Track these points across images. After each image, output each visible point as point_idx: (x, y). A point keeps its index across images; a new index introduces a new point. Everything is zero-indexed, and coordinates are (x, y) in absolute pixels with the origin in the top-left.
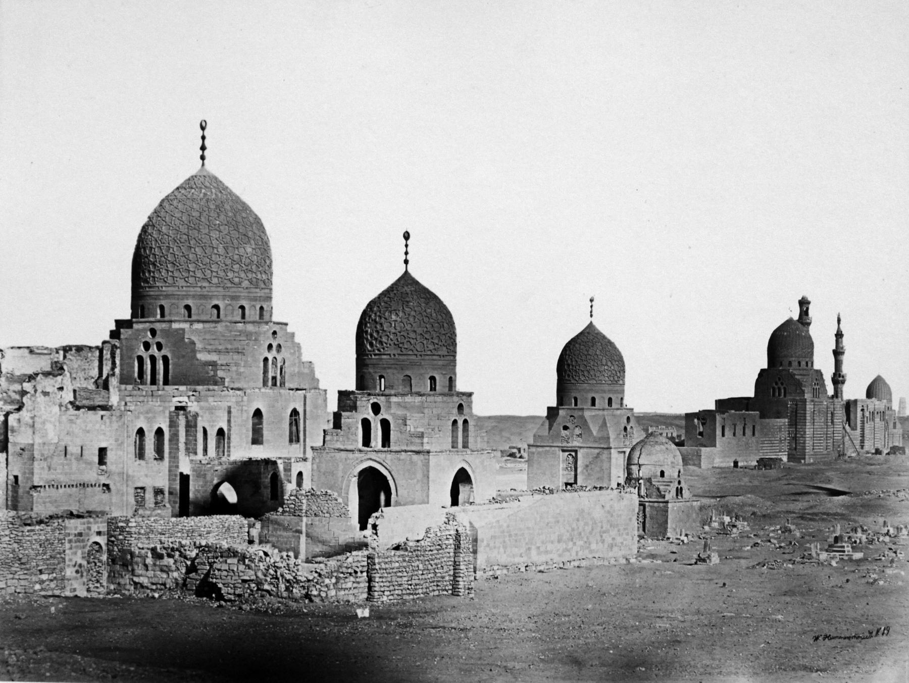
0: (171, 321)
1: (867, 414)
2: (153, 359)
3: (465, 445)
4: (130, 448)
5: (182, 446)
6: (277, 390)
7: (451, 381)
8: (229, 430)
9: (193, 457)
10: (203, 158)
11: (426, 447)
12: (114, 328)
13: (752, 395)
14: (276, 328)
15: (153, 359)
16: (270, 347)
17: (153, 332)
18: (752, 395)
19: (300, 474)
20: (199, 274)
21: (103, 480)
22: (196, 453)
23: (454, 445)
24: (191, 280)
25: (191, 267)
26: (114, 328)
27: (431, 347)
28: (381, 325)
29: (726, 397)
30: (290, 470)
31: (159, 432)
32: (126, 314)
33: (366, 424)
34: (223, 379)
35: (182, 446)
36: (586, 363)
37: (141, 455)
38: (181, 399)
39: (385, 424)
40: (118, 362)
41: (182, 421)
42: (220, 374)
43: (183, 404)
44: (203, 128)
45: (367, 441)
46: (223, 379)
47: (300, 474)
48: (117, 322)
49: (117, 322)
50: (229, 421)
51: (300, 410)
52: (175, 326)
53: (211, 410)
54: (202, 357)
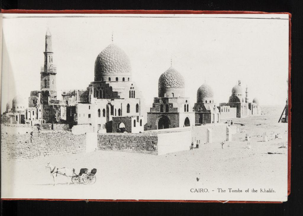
1: (253, 106)
2: (101, 91)
3: (188, 111)
6: (133, 99)
8: (122, 109)
9: (112, 116)
16: (131, 88)
20: (112, 69)
22: (113, 115)
25: (111, 68)
27: (179, 85)
28: (165, 80)
30: (138, 119)
31: (104, 110)
34: (119, 96)
38: (109, 101)
42: (119, 95)
43: (110, 102)
46: (119, 96)
50: (121, 107)
53: (116, 104)
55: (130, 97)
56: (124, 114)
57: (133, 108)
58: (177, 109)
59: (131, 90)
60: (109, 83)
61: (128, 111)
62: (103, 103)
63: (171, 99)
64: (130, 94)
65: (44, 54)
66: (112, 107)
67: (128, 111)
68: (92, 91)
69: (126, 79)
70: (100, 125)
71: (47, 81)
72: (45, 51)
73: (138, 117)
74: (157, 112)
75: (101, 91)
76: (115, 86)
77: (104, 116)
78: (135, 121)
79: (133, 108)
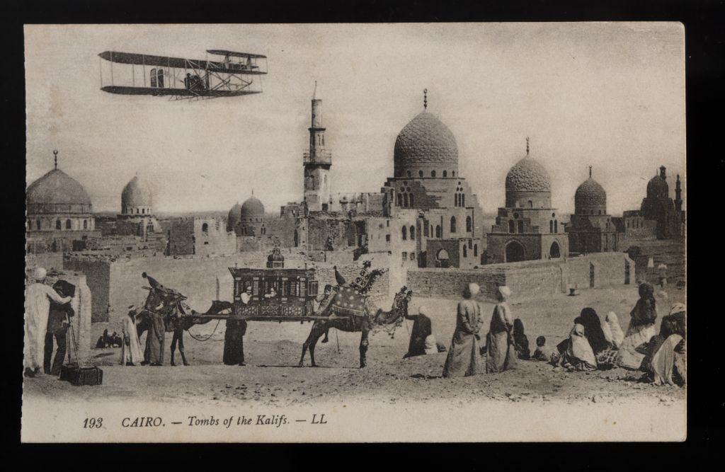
3: (556, 231)
4: (400, 235)
5: (422, 233)
7: (605, 212)
10: (528, 147)
11: (540, 233)
12: (386, 181)
13: (33, 33)
14: (460, 180)
15: (405, 195)
17: (405, 183)
18: (33, 33)
19: (476, 245)
20: (426, 157)
21: (389, 249)
23: (551, 231)
24: (422, 160)
26: (386, 181)
29: (26, 78)
31: (412, 228)
32: (392, 176)
33: (511, 222)
35: (422, 233)
36: (589, 198)
37: (404, 238)
39: (521, 223)
40: (394, 195)
41: (422, 222)
44: (425, 93)
45: (512, 230)
47: (476, 245)
48: (388, 179)
49: (388, 179)
50: (442, 222)
51: (471, 217)
53: (433, 217)
54: (429, 194)
55: (456, 205)
56: (447, 234)
57: (461, 224)
58: (537, 227)
59: (458, 193)
61: (453, 230)
62: (409, 217)
63: (527, 211)
64: (456, 201)
66: (426, 223)
67: (453, 230)
68: (392, 197)
69: (449, 175)
70: (406, 253)
71: (315, 178)
72: (310, 126)
73: (470, 241)
74: (504, 233)
75: (405, 195)
76: (432, 187)
77: (412, 238)
78: (465, 247)
79: (461, 224)
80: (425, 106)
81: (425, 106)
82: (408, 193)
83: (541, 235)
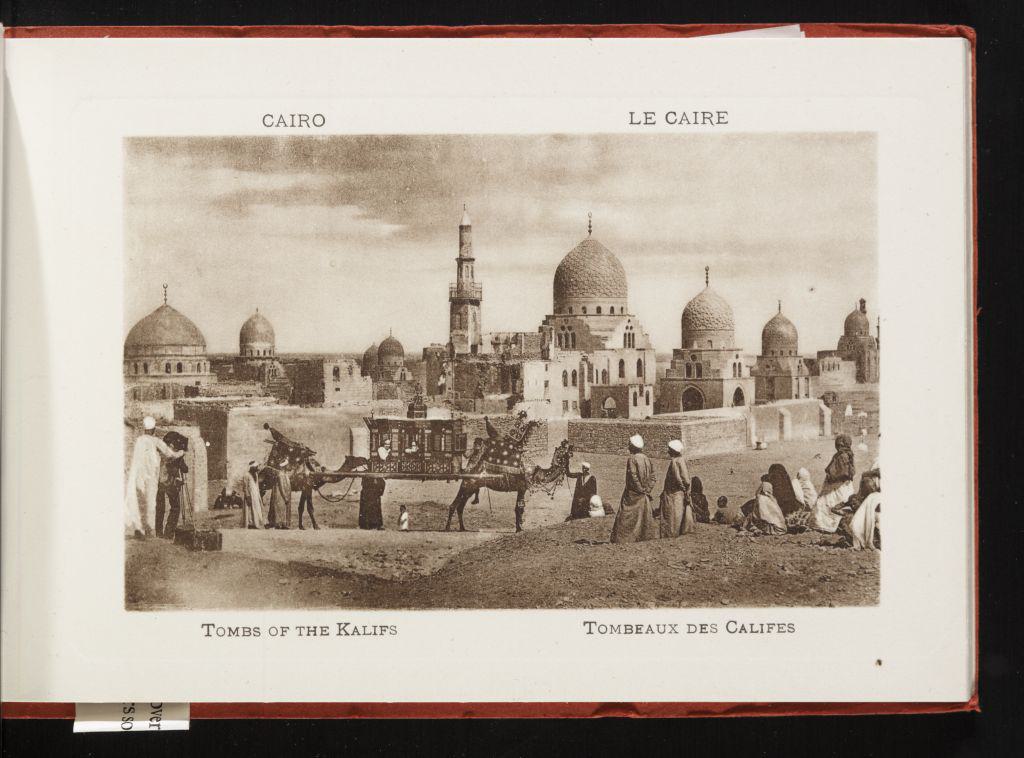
0: (575, 316)
2: (566, 335)
3: (740, 375)
16: (627, 328)
23: (734, 375)
31: (574, 374)
35: (586, 379)
52: (578, 318)
59: (627, 332)
60: (584, 318)
65: (456, 263)
69: (617, 311)
80: (590, 232)
81: (590, 232)
82: (570, 333)
83: (722, 380)
